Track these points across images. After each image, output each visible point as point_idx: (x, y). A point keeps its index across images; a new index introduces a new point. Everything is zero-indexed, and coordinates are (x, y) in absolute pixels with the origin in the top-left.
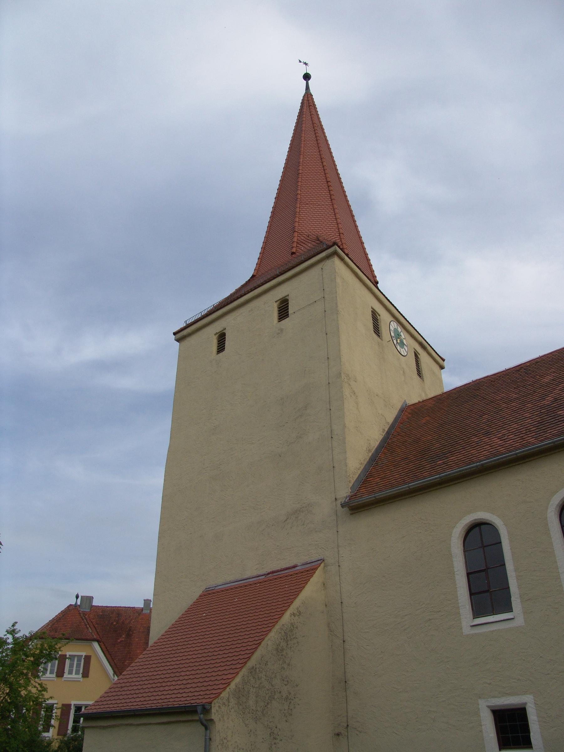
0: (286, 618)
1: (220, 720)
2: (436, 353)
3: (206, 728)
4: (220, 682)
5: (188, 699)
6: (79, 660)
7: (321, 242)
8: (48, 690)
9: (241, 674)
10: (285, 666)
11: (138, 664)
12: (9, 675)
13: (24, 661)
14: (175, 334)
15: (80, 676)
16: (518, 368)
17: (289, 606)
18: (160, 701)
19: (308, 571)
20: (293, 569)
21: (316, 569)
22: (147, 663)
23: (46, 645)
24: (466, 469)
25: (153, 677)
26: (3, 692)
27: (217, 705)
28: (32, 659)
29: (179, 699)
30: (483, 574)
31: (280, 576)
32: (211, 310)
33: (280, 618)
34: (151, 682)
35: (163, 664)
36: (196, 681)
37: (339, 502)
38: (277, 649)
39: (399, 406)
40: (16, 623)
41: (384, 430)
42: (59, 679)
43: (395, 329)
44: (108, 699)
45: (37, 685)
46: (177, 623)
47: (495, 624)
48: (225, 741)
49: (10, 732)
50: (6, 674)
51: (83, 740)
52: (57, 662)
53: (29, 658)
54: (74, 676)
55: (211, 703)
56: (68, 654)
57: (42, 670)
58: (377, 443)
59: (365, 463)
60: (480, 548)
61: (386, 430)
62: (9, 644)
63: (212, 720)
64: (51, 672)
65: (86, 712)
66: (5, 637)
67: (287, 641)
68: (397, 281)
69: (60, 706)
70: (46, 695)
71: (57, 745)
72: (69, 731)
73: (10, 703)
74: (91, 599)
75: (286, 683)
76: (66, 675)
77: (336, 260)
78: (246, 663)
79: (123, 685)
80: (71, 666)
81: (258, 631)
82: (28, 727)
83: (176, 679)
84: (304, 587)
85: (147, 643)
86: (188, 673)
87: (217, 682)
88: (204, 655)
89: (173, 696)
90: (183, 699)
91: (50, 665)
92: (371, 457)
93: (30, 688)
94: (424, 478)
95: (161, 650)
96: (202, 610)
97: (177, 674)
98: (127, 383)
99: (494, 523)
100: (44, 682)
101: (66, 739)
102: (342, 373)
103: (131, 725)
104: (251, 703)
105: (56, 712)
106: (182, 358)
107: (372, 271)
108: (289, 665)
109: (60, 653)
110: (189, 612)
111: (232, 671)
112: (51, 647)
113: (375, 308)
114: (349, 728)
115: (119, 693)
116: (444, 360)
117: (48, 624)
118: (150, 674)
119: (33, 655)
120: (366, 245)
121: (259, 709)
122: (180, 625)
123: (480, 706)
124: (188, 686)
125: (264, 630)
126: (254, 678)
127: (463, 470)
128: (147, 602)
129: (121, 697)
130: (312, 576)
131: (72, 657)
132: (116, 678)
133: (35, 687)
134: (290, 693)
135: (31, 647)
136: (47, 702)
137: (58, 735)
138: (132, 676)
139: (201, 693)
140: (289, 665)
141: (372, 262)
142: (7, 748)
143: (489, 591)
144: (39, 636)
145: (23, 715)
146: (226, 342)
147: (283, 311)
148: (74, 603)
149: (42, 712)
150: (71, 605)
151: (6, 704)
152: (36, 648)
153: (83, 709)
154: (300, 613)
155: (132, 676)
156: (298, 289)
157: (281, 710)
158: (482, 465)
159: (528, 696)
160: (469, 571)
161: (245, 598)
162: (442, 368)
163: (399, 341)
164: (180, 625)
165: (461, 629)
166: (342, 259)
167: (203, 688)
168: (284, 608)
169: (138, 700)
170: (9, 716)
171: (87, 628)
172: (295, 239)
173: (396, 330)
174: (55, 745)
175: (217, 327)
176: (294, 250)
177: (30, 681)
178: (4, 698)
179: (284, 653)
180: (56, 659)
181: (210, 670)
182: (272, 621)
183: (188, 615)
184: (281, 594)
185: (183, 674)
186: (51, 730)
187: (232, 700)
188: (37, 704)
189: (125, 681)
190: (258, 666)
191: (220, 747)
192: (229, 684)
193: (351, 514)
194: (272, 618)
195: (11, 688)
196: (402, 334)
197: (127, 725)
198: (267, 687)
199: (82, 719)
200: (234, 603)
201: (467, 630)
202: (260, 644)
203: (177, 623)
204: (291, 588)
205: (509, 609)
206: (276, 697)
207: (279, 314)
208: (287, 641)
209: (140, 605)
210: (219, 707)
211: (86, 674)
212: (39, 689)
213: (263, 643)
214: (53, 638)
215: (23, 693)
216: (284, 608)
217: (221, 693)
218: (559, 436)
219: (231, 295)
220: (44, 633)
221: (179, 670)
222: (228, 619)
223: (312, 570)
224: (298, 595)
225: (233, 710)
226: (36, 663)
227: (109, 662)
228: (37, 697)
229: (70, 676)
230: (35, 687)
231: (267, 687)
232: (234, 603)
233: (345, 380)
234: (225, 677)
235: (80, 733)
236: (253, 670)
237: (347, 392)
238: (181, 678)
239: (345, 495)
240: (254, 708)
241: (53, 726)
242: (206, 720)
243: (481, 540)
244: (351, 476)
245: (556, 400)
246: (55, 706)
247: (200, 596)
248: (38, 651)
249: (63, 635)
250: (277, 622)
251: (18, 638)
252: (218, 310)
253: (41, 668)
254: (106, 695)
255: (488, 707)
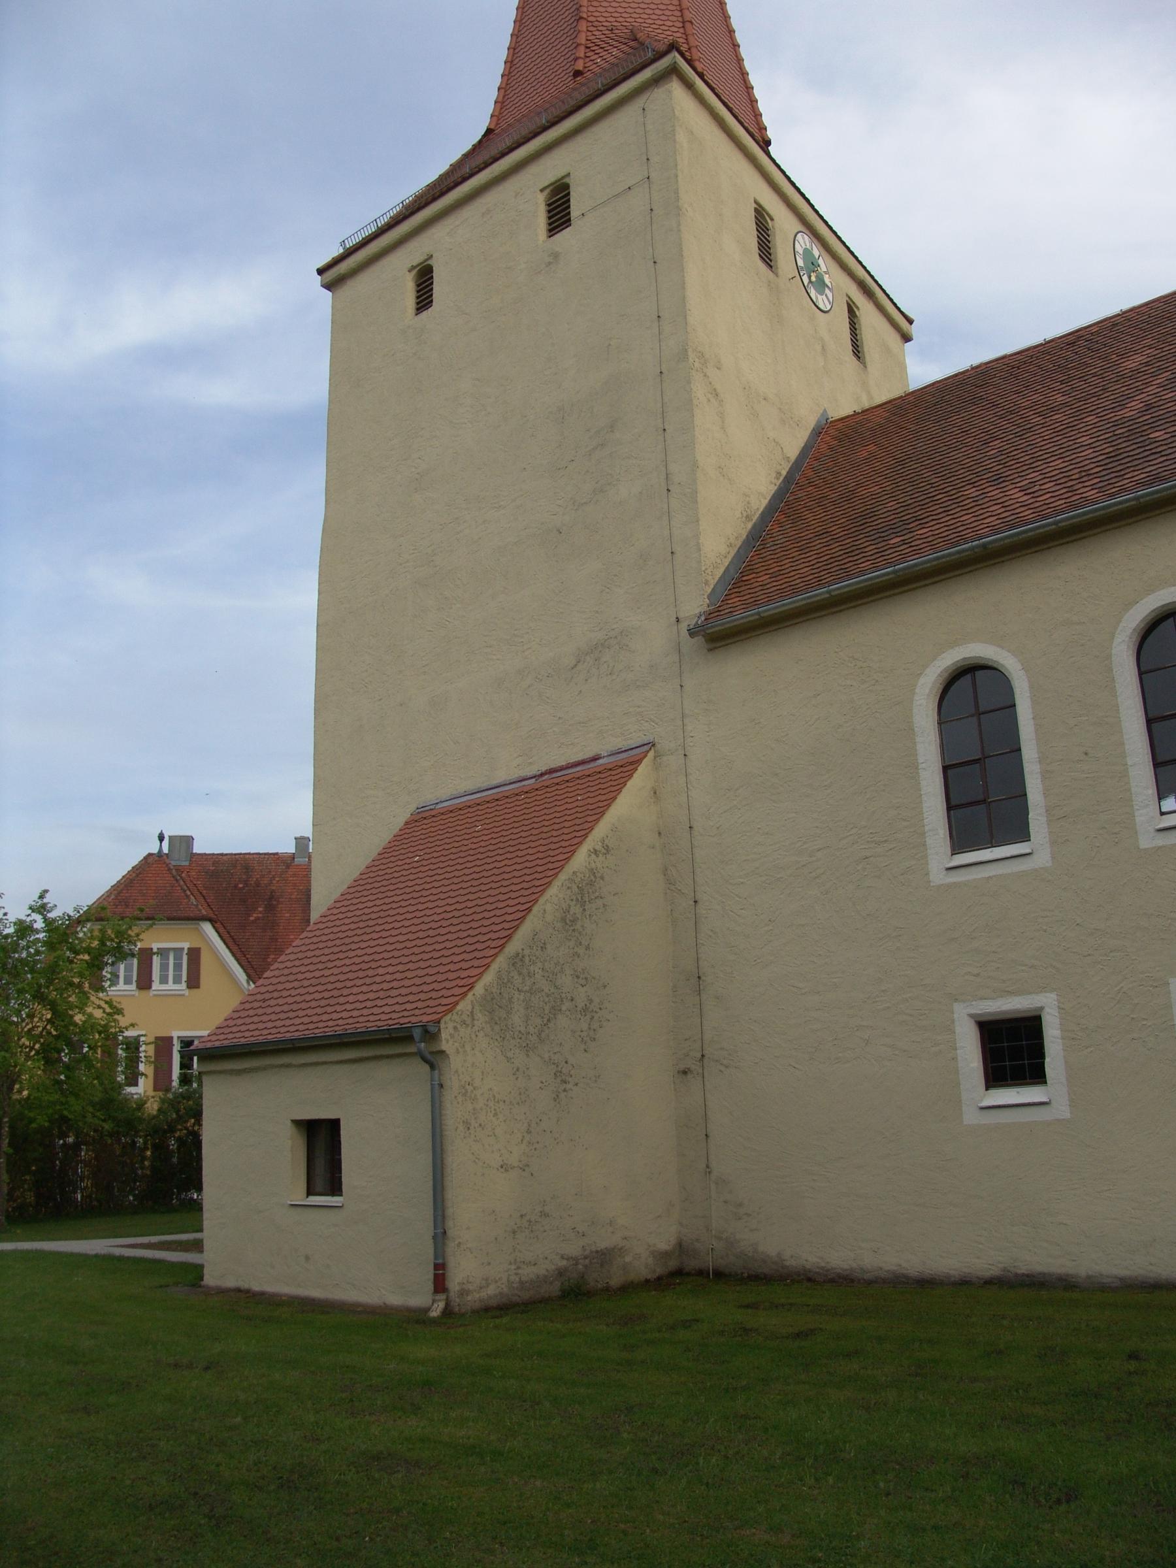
0: (580, 859)
1: (458, 1052)
2: (895, 304)
3: (432, 1067)
4: (454, 983)
5: (394, 1016)
6: (178, 958)
7: (642, 44)
8: (125, 1012)
9: (495, 966)
10: (581, 951)
11: (292, 957)
12: (48, 987)
13: (71, 962)
14: (320, 272)
15: (184, 986)
16: (1072, 338)
17: (586, 836)
18: (340, 1022)
19: (621, 768)
20: (592, 765)
21: (639, 761)
22: (309, 954)
23: (109, 932)
24: (950, 555)
25: (323, 980)
26: (40, 1019)
27: (451, 1025)
28: (87, 957)
29: (378, 1017)
30: (981, 710)
31: (566, 778)
32: (399, 214)
33: (568, 859)
34: (320, 988)
35: (341, 956)
36: (407, 983)
37: (684, 627)
38: (563, 920)
39: (811, 422)
40: (46, 891)
41: (779, 473)
42: (144, 992)
43: (806, 250)
44: (239, 1022)
45: (102, 1004)
46: (364, 877)
47: (994, 865)
48: (470, 1088)
49: (65, 1086)
50: (40, 986)
51: (201, 1097)
52: (135, 961)
53: (81, 957)
54: (171, 985)
55: (439, 1022)
56: (155, 947)
57: (109, 976)
58: (765, 502)
59: (739, 543)
60: (972, 716)
61: (784, 473)
62: (37, 931)
63: (443, 1052)
64: (128, 981)
65: (201, 1046)
66: (28, 919)
67: (583, 904)
68: (808, 140)
69: (152, 1040)
70: (123, 1021)
71: (156, 1107)
72: (175, 1083)
73: (57, 1037)
74: (188, 840)
75: (583, 982)
76: (156, 985)
77: (675, 87)
78: (503, 946)
79: (267, 996)
80: (164, 967)
81: (525, 885)
82: (97, 1078)
83: (368, 981)
84: (615, 798)
85: (308, 921)
86: (391, 969)
87: (448, 984)
88: (421, 934)
89: (365, 1012)
90: (383, 1017)
91: (122, 967)
92: (750, 532)
93: (89, 1010)
94: (863, 573)
95: (335, 930)
96: (412, 849)
97: (371, 973)
98: (221, 392)
99: (1003, 666)
100: (114, 999)
101: (170, 1096)
102: (690, 350)
103: (288, 1066)
104: (517, 1019)
105: (147, 1051)
106: (340, 327)
107: (758, 115)
108: (587, 948)
109: (139, 945)
110: (386, 855)
111: (476, 963)
112: (121, 935)
113: (762, 203)
114: (705, 1061)
115: (260, 1011)
116: (911, 322)
117: (109, 893)
118: (317, 974)
119: (88, 950)
120: (743, 52)
121: (532, 1030)
122: (370, 881)
123: (956, 1016)
124: (394, 993)
125: (537, 883)
126: (520, 974)
127: (943, 557)
128: (301, 842)
129: (265, 1018)
130: (631, 776)
131: (163, 953)
132: (253, 986)
133: (99, 1007)
134: (591, 1001)
135: (81, 935)
136: (127, 1034)
137: (155, 1089)
138: (282, 979)
139: (419, 1005)
140: (587, 948)
141: (757, 93)
142: (65, 1113)
143: (985, 798)
144: (95, 914)
145: (85, 1056)
146: (435, 286)
147: (559, 212)
148: (156, 851)
149: (120, 1052)
150: (150, 855)
151: (51, 1039)
152: (92, 938)
153: (196, 1043)
154: (607, 850)
155: (282, 979)
156: (590, 160)
157: (574, 1032)
158: (984, 546)
159: (1048, 994)
160: (947, 763)
161: (497, 824)
162: (907, 338)
163: (813, 279)
164: (370, 881)
165: (927, 874)
166: (689, 86)
167: (422, 996)
168: (576, 841)
169: (298, 1021)
170: (60, 1060)
171: (188, 896)
172: (582, 39)
173: (807, 252)
174: (152, 1107)
175: (412, 254)
176: (579, 66)
177: (88, 998)
178: (44, 1028)
179: (578, 927)
180: (133, 955)
181: (433, 962)
182: (551, 866)
183: (384, 861)
184: (569, 812)
185: (381, 971)
186: (141, 1081)
187: (479, 1015)
188: (107, 1038)
189: (271, 988)
190: (527, 952)
191: (460, 1099)
192: (471, 987)
193: (710, 650)
194: (553, 860)
195: (55, 1012)
196: (821, 262)
197: (282, 1066)
198: (546, 990)
199: (195, 1058)
200: (476, 834)
201: (938, 877)
202: (529, 910)
203: (364, 877)
204: (590, 801)
205: (1021, 833)
206: (564, 1008)
207: (550, 218)
208: (583, 904)
209: (288, 847)
210: (455, 1028)
211: (194, 982)
212: (108, 1010)
213: (535, 909)
214: (122, 919)
215: (79, 1018)
216: (576, 841)
217: (457, 1003)
218: (1150, 484)
219: (442, 178)
220: (103, 909)
221: (374, 965)
222: (461, 913)
223: (631, 763)
224: (603, 813)
225: (481, 1034)
226: (96, 965)
227: (237, 960)
228: (105, 1026)
229: (164, 987)
230: (99, 1007)
231: (546, 990)
232: (476, 834)
233: (696, 364)
234: (464, 974)
235: (195, 1085)
236: (517, 960)
237: (699, 391)
238: (378, 979)
239: (697, 611)
240: (522, 1029)
241: (142, 1074)
242: (432, 1053)
243: (975, 700)
244: (708, 571)
245: (1149, 407)
246: (142, 1039)
247: (407, 823)
248: (96, 943)
249: (142, 910)
250: (562, 867)
251: (54, 920)
252: (412, 213)
253: (106, 973)
254: (236, 1015)
255: (971, 1016)
